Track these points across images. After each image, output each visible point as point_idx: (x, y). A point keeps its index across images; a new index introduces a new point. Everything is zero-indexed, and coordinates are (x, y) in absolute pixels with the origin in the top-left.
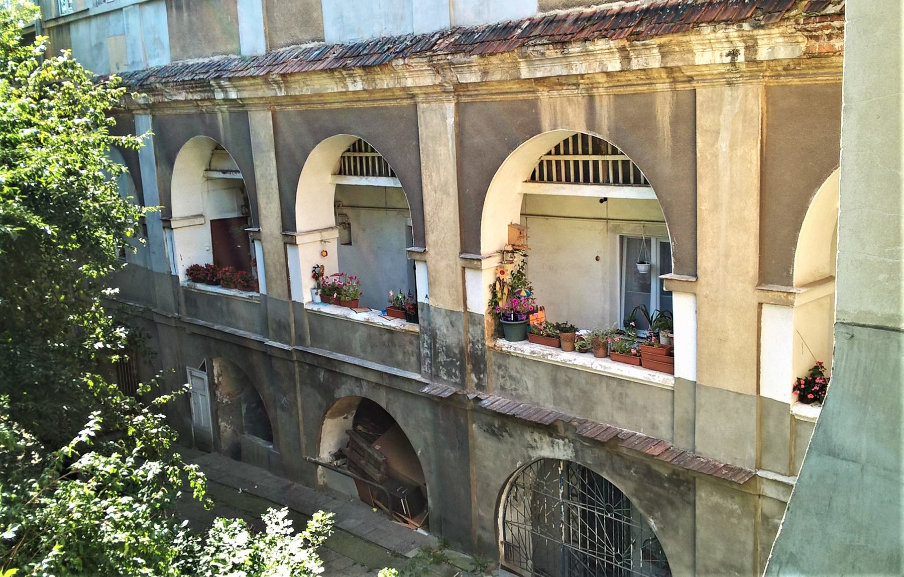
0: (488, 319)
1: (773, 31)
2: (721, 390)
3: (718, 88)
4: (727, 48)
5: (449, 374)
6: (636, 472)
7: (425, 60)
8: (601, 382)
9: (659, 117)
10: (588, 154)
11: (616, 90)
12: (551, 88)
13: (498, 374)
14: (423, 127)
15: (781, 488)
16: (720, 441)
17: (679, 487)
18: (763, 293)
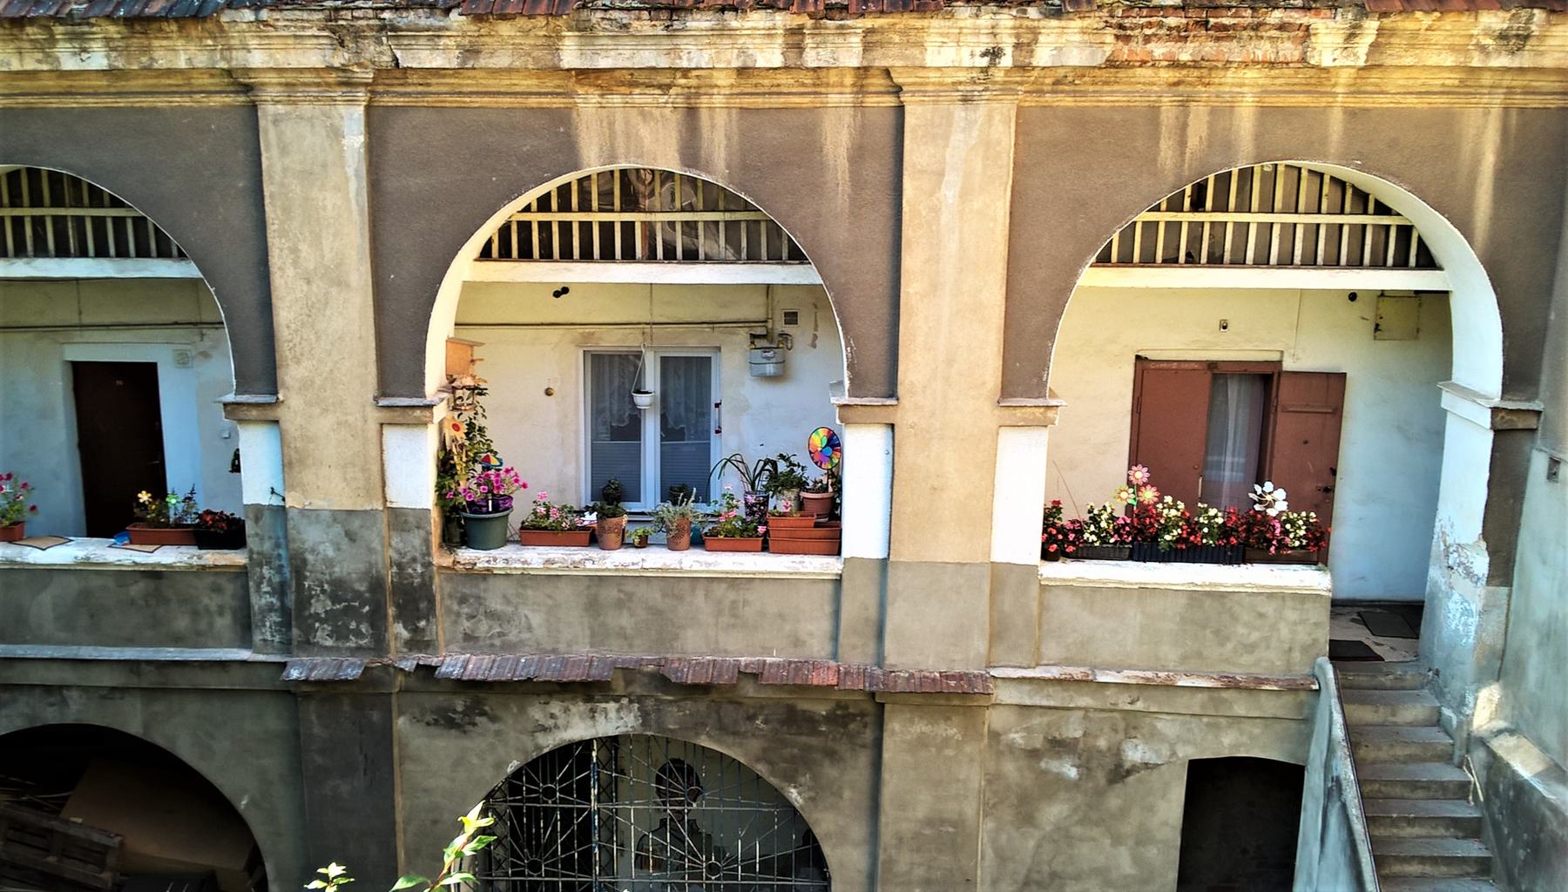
0: (435, 516)
1: (1072, 24)
2: (933, 564)
3: (943, 107)
4: (985, 42)
5: (340, 634)
6: (766, 722)
7: (321, 16)
8: (693, 590)
9: (829, 148)
10: (590, 210)
11: (748, 102)
12: (606, 91)
13: (458, 615)
14: (275, 152)
15: (1026, 688)
16: (922, 644)
17: (845, 726)
18: (1007, 412)
